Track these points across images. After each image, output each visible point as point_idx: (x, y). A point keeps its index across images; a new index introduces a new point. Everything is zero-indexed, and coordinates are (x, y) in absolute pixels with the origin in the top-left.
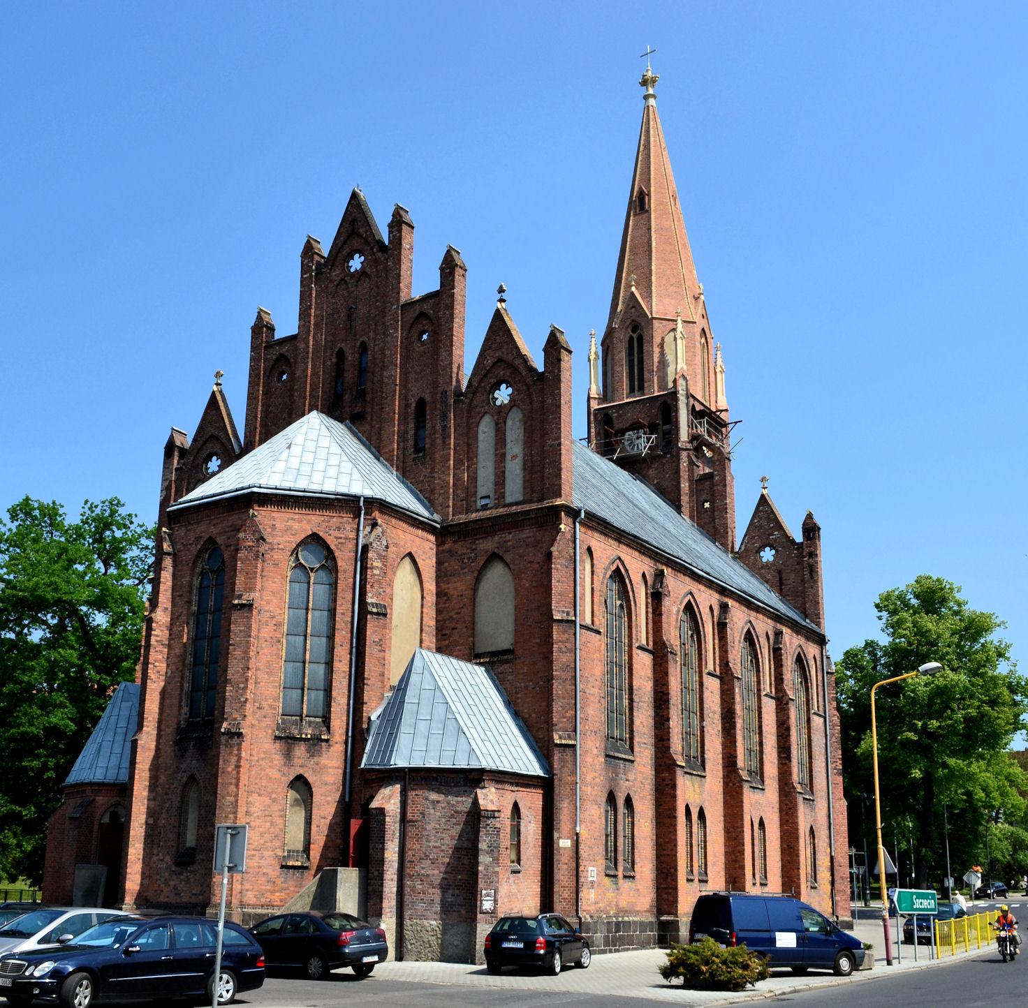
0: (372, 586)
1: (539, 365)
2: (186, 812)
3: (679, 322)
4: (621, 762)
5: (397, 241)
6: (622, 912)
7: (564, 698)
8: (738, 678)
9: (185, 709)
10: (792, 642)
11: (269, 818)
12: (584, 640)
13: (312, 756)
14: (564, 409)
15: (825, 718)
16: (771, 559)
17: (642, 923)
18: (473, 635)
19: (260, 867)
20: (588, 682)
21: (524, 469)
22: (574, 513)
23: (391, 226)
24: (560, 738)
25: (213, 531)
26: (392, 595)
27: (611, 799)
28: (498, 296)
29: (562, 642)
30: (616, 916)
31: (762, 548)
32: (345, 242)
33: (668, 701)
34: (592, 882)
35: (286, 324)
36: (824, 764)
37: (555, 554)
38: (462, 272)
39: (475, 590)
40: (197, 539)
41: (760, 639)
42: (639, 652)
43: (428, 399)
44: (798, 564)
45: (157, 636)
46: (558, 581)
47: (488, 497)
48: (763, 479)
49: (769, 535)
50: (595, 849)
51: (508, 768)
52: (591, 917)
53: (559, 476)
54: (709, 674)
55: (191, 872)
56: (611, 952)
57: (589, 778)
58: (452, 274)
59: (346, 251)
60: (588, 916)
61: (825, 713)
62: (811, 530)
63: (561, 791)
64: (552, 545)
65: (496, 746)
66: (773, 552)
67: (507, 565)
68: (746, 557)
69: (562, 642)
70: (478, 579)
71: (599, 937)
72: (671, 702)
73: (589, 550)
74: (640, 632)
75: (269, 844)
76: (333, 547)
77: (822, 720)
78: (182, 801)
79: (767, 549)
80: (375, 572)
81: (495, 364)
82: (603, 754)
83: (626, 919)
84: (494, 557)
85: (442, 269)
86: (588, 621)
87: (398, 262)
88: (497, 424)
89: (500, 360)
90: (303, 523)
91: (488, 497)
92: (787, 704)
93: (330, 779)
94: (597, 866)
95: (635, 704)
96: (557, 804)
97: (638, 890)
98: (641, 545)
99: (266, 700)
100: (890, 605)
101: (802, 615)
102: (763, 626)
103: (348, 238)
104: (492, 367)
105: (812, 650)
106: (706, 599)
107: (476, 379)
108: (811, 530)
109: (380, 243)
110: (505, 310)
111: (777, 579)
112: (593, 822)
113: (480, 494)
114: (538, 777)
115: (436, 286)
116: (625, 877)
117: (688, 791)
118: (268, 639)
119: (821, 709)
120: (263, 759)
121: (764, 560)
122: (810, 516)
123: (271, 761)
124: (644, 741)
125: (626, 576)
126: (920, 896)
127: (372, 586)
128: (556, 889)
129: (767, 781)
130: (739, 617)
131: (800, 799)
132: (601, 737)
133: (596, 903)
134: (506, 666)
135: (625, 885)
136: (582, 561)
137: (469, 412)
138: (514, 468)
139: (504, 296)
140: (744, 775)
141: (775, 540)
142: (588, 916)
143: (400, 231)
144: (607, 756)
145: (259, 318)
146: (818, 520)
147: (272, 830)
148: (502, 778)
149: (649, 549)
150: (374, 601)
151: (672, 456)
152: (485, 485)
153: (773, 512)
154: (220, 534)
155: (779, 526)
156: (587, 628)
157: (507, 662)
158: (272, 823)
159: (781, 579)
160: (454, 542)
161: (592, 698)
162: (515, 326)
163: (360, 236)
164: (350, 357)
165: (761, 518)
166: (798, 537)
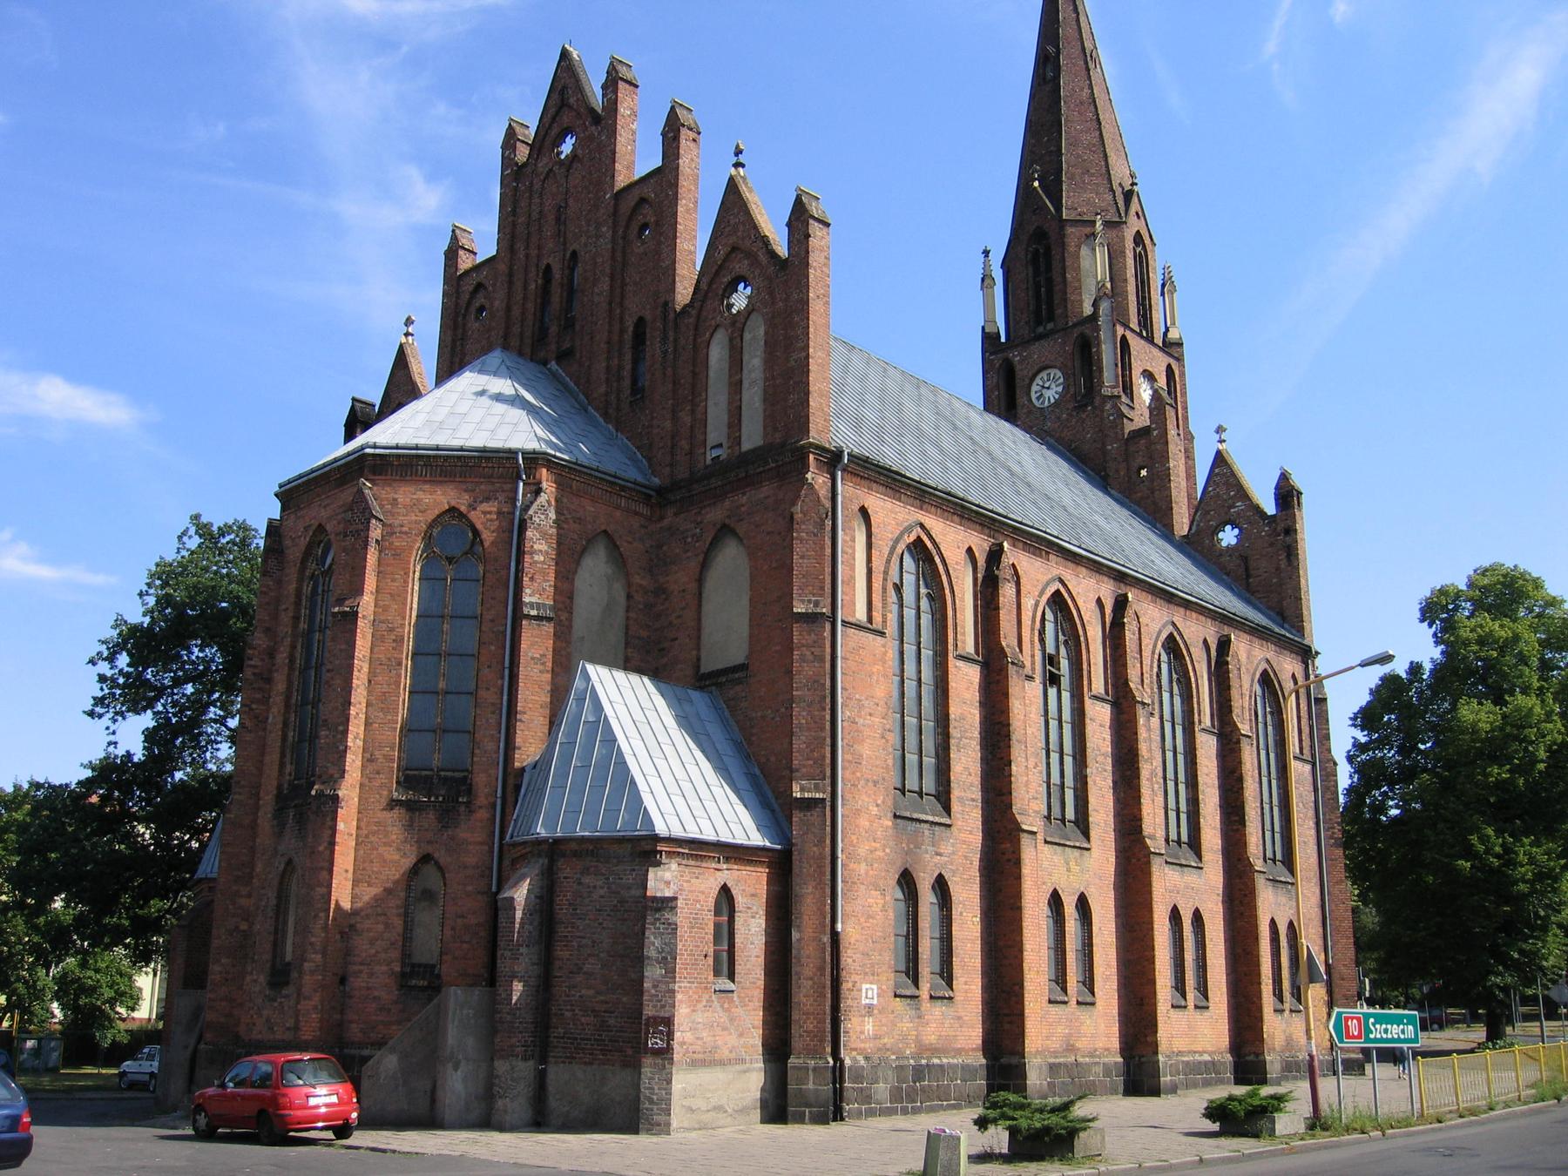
0: (532, 579)
1: (782, 250)
2: (286, 913)
3: (1099, 226)
4: (926, 826)
5: (612, 106)
6: (923, 1049)
7: (809, 729)
8: (1143, 704)
9: (289, 768)
10: (1248, 656)
11: (382, 918)
12: (851, 644)
13: (445, 827)
14: (815, 307)
15: (1314, 765)
16: (1234, 541)
17: (965, 1067)
18: (698, 649)
19: (368, 988)
20: (861, 707)
21: (765, 400)
22: (832, 459)
23: (604, 87)
24: (802, 790)
25: (324, 514)
26: (572, 593)
27: (907, 881)
28: (734, 160)
29: (808, 646)
30: (917, 1056)
31: (1220, 527)
32: (554, 119)
33: (1008, 736)
34: (870, 1007)
35: (484, 241)
36: (1313, 832)
37: (798, 516)
38: (692, 135)
39: (700, 581)
40: (306, 528)
41: (1192, 650)
42: (960, 664)
43: (648, 317)
44: (1272, 545)
45: (255, 667)
46: (802, 557)
47: (720, 445)
48: (1220, 430)
49: (1230, 507)
50: (876, 957)
51: (709, 835)
52: (867, 1058)
53: (805, 403)
54: (1096, 697)
55: (286, 996)
56: (905, 1112)
57: (862, 850)
58: (676, 138)
59: (555, 131)
60: (860, 1058)
61: (1313, 756)
62: (1287, 495)
63: (803, 868)
64: (794, 504)
65: (695, 803)
66: (1236, 531)
67: (741, 540)
68: (1198, 547)
69: (808, 646)
70: (704, 566)
71: (882, 1089)
72: (1014, 737)
73: (864, 511)
74: (964, 634)
75: (383, 955)
76: (479, 526)
77: (1308, 767)
78: (279, 898)
79: (1228, 528)
80: (536, 558)
81: (728, 255)
82: (890, 815)
83: (936, 1061)
84: (725, 531)
85: (664, 134)
86: (861, 615)
87: (613, 133)
88: (731, 340)
89: (734, 249)
90: (436, 498)
91: (720, 445)
92: (1238, 742)
93: (471, 860)
94: (878, 982)
95: (952, 741)
96: (796, 889)
97: (959, 1018)
98: (963, 507)
99: (381, 747)
100: (1438, 610)
101: (1279, 619)
102: (1197, 632)
103: (557, 113)
104: (724, 261)
105: (1288, 666)
106: (1088, 592)
107: (705, 280)
108: (1287, 495)
109: (592, 111)
110: (744, 178)
111: (1234, 571)
112: (870, 917)
113: (710, 443)
114: (764, 849)
115: (657, 162)
116: (1196, 1007)
117: (1046, 869)
118: (384, 661)
119: (1306, 751)
120: (374, 833)
121: (1224, 544)
122: (1284, 477)
123: (386, 834)
124: (970, 795)
125: (934, 552)
126: (1379, 1020)
127: (532, 579)
128: (795, 1016)
129: (1206, 855)
130: (1150, 619)
131: (1260, 881)
132: (886, 789)
133: (877, 1037)
134: (738, 688)
135: (936, 1011)
136: (848, 529)
137: (696, 329)
138: (753, 398)
139: (742, 159)
140: (1156, 843)
141: (1238, 513)
142: (860, 1058)
143: (616, 92)
144: (895, 816)
145: (454, 238)
146: (1297, 481)
147: (386, 935)
148: (698, 849)
149: (977, 513)
150: (534, 600)
151: (1094, 408)
152: (716, 431)
153: (1233, 474)
154: (329, 519)
155: (1243, 494)
156: (859, 627)
157: (739, 682)
158: (387, 925)
159: (1247, 569)
160: (675, 514)
161: (867, 732)
162: (756, 199)
163: (570, 107)
164: (557, 274)
165: (1218, 485)
166: (1270, 508)
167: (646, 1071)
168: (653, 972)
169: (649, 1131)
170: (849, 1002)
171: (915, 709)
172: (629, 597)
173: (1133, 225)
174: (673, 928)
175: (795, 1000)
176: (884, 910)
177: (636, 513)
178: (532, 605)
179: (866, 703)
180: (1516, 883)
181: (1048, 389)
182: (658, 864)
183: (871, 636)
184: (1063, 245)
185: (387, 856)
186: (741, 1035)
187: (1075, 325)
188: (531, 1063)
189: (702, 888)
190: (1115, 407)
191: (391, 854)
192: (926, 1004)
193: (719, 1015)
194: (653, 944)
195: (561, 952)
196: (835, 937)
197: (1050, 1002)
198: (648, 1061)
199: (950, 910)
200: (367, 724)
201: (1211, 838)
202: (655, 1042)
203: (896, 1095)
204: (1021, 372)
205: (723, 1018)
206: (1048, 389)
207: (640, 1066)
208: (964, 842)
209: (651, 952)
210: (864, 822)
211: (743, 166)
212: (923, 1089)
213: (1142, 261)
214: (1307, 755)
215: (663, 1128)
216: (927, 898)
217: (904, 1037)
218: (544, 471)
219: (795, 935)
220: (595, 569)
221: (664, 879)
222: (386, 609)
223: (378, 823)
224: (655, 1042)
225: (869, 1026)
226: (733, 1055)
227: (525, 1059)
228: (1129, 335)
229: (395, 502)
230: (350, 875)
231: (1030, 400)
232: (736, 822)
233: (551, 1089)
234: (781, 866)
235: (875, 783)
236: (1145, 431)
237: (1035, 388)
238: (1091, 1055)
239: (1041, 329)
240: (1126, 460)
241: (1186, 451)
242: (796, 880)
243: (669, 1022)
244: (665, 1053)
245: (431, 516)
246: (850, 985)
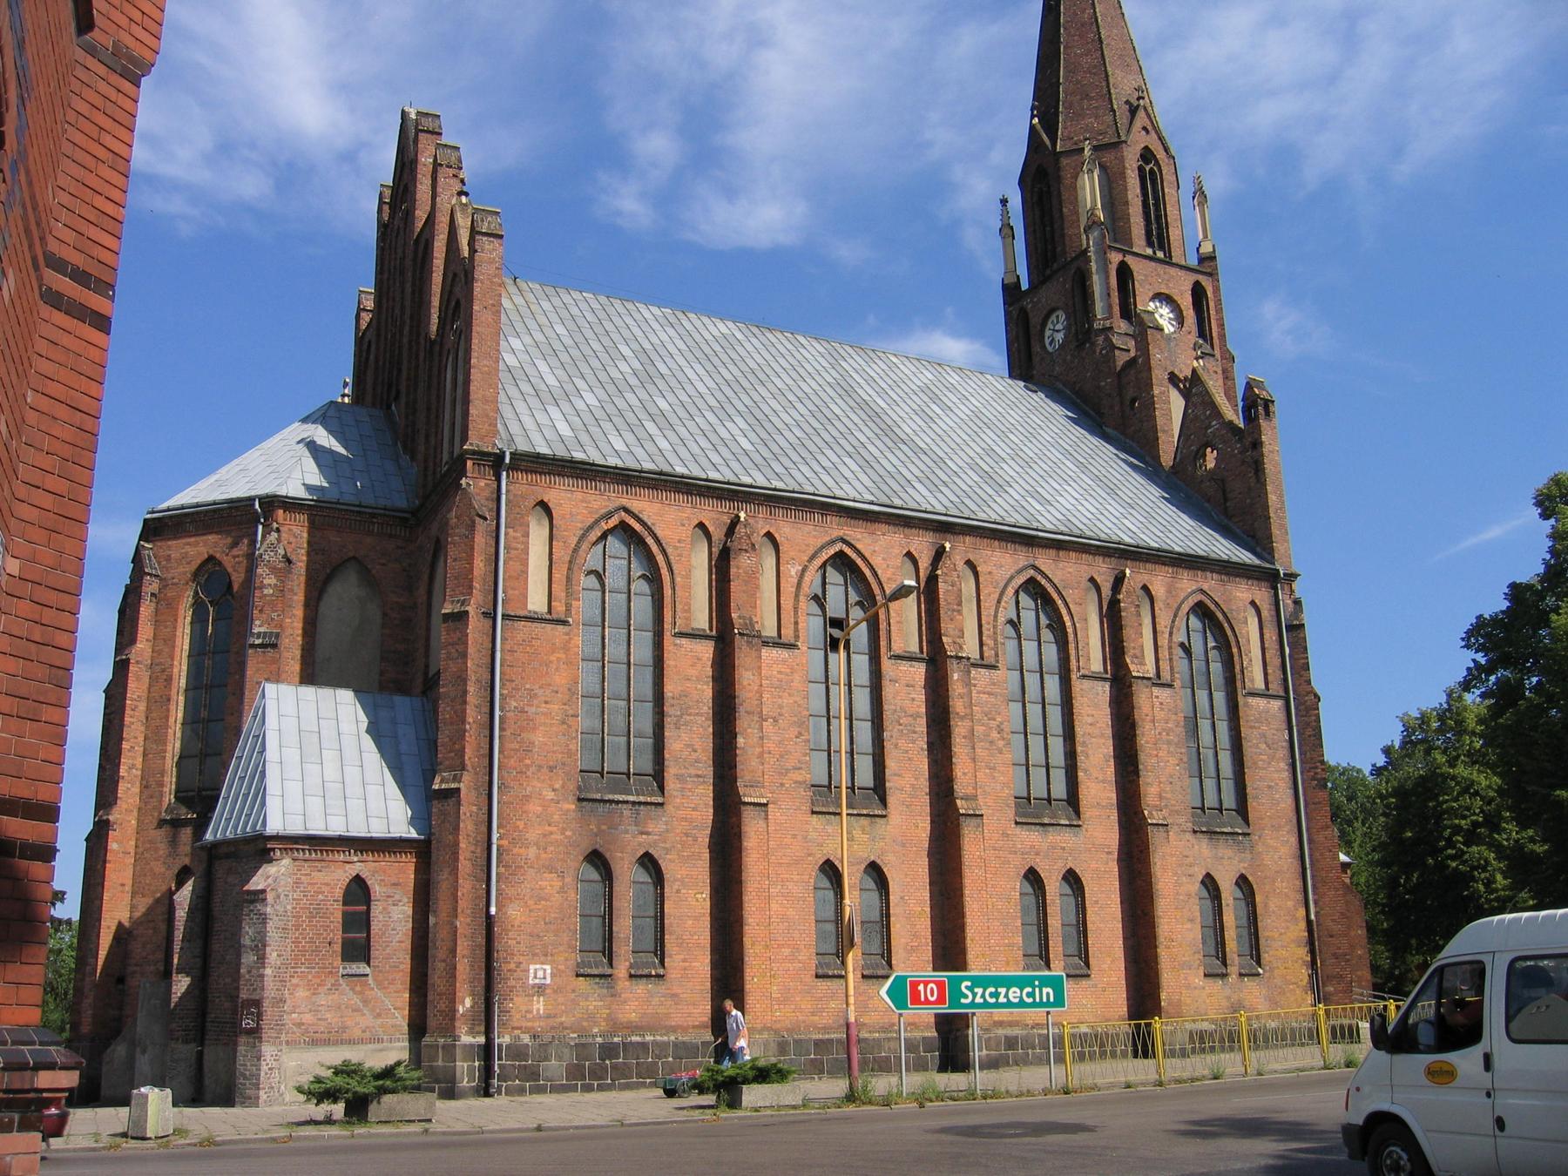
6: (615, 1026)
22: (495, 462)
36: (1286, 775)
50: (550, 938)
57: (532, 835)
71: (555, 1067)
77: (1277, 705)
82: (572, 798)
97: (675, 995)
112: (541, 899)
123: (156, 850)
144: (580, 800)
150: (262, 630)
167: (241, 1049)
168: (248, 959)
169: (243, 1104)
170: (512, 983)
171: (1204, 678)
172: (385, 614)
173: (1137, 141)
174: (264, 919)
175: (430, 982)
176: (562, 890)
177: (391, 536)
178: (259, 635)
179: (540, 692)
180: (1513, 819)
181: (1056, 332)
182: (270, 861)
183: (549, 626)
184: (1059, 179)
185: (157, 870)
186: (379, 1015)
187: (1073, 259)
188: (193, 1045)
189: (327, 879)
190: (1108, 340)
191: (159, 868)
192: (623, 983)
193: (348, 996)
194: (248, 932)
195: (216, 946)
196: (489, 921)
197: (817, 976)
198: (242, 1039)
199: (662, 888)
200: (145, 755)
201: (1099, 787)
202: (248, 1023)
203: (575, 1072)
204: (1035, 320)
205: (356, 1000)
206: (1056, 332)
207: (236, 1044)
208: (685, 819)
209: (246, 941)
210: (534, 807)
211: (466, 194)
212: (614, 1067)
213: (1151, 179)
214: (1276, 688)
215: (253, 1101)
216: (628, 875)
217: (591, 1017)
218: (281, 512)
219: (432, 920)
220: (345, 592)
221: (274, 876)
222: (160, 652)
223: (151, 842)
224: (248, 1023)
225: (539, 1005)
226: (368, 1035)
227: (186, 1042)
228: (1130, 260)
229: (168, 558)
230: (128, 888)
231: (1044, 347)
232: (389, 813)
233: (206, 1070)
234: (426, 852)
235: (551, 769)
236: (1133, 361)
237: (1048, 333)
238: (884, 1029)
239: (1048, 272)
240: (1120, 395)
241: (1224, 371)
242: (434, 867)
243: (258, 1003)
244: (255, 1032)
245: (195, 566)
246: (512, 966)
